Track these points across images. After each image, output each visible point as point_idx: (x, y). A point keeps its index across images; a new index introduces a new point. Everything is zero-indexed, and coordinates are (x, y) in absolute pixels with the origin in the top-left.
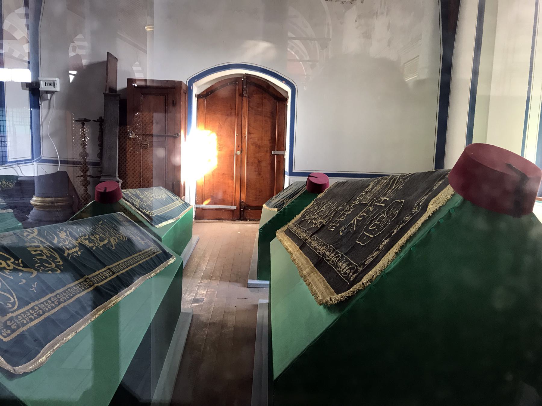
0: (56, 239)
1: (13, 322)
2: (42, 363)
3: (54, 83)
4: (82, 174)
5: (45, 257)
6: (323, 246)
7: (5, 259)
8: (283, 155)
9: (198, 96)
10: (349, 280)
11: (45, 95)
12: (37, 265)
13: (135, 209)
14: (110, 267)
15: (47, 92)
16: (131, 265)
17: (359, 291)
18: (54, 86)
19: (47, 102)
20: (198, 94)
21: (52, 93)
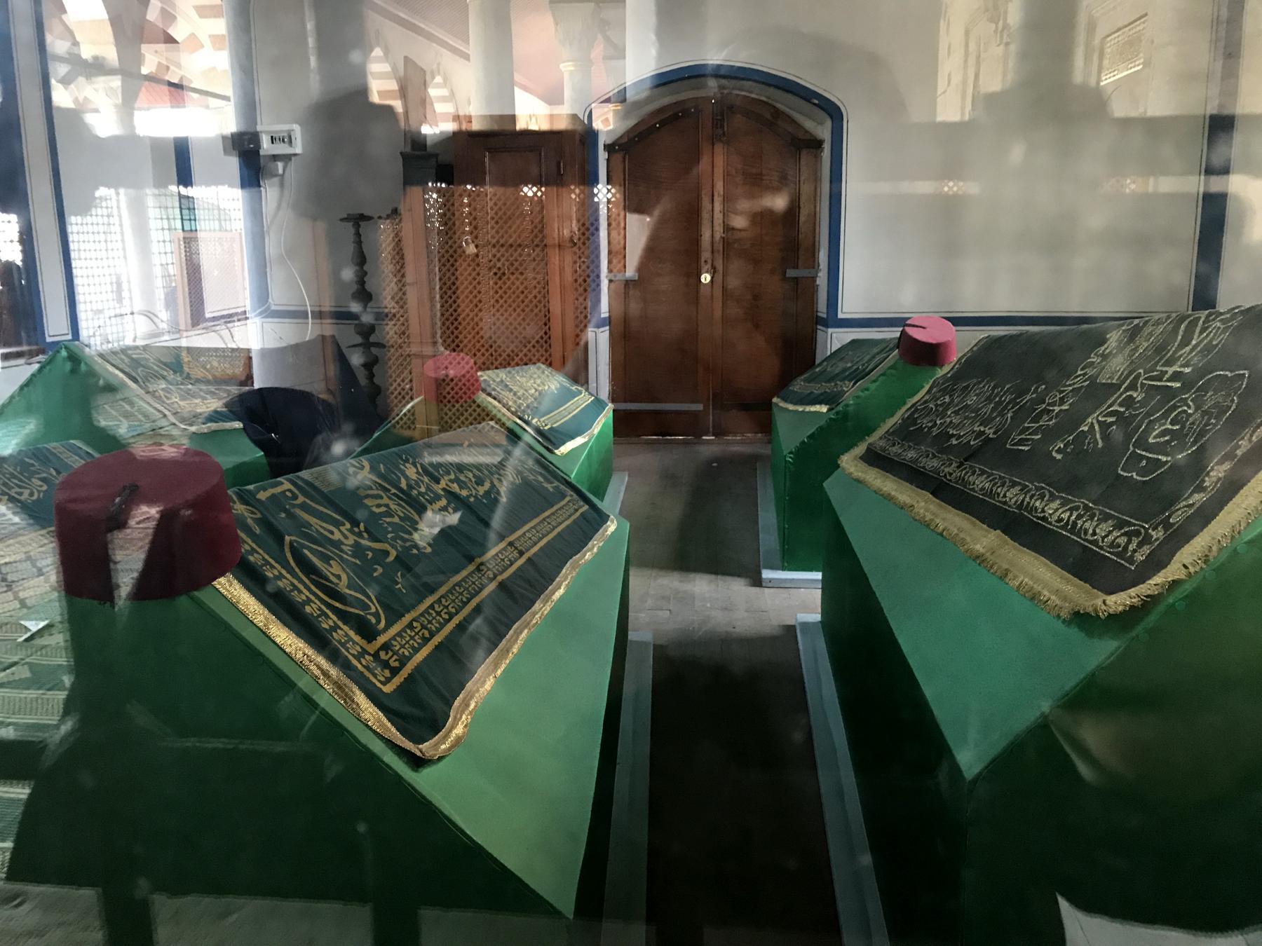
0: (403, 480)
1: (390, 653)
2: (459, 739)
3: (290, 137)
4: (359, 340)
5: (396, 520)
6: (1013, 486)
7: (338, 524)
8: (814, 279)
9: (608, 148)
10: (1131, 560)
11: (271, 165)
12: (390, 536)
13: (509, 414)
14: (511, 538)
15: (275, 158)
16: (544, 536)
17: (1175, 584)
18: (290, 142)
19: (276, 180)
20: (609, 142)
21: (287, 158)
